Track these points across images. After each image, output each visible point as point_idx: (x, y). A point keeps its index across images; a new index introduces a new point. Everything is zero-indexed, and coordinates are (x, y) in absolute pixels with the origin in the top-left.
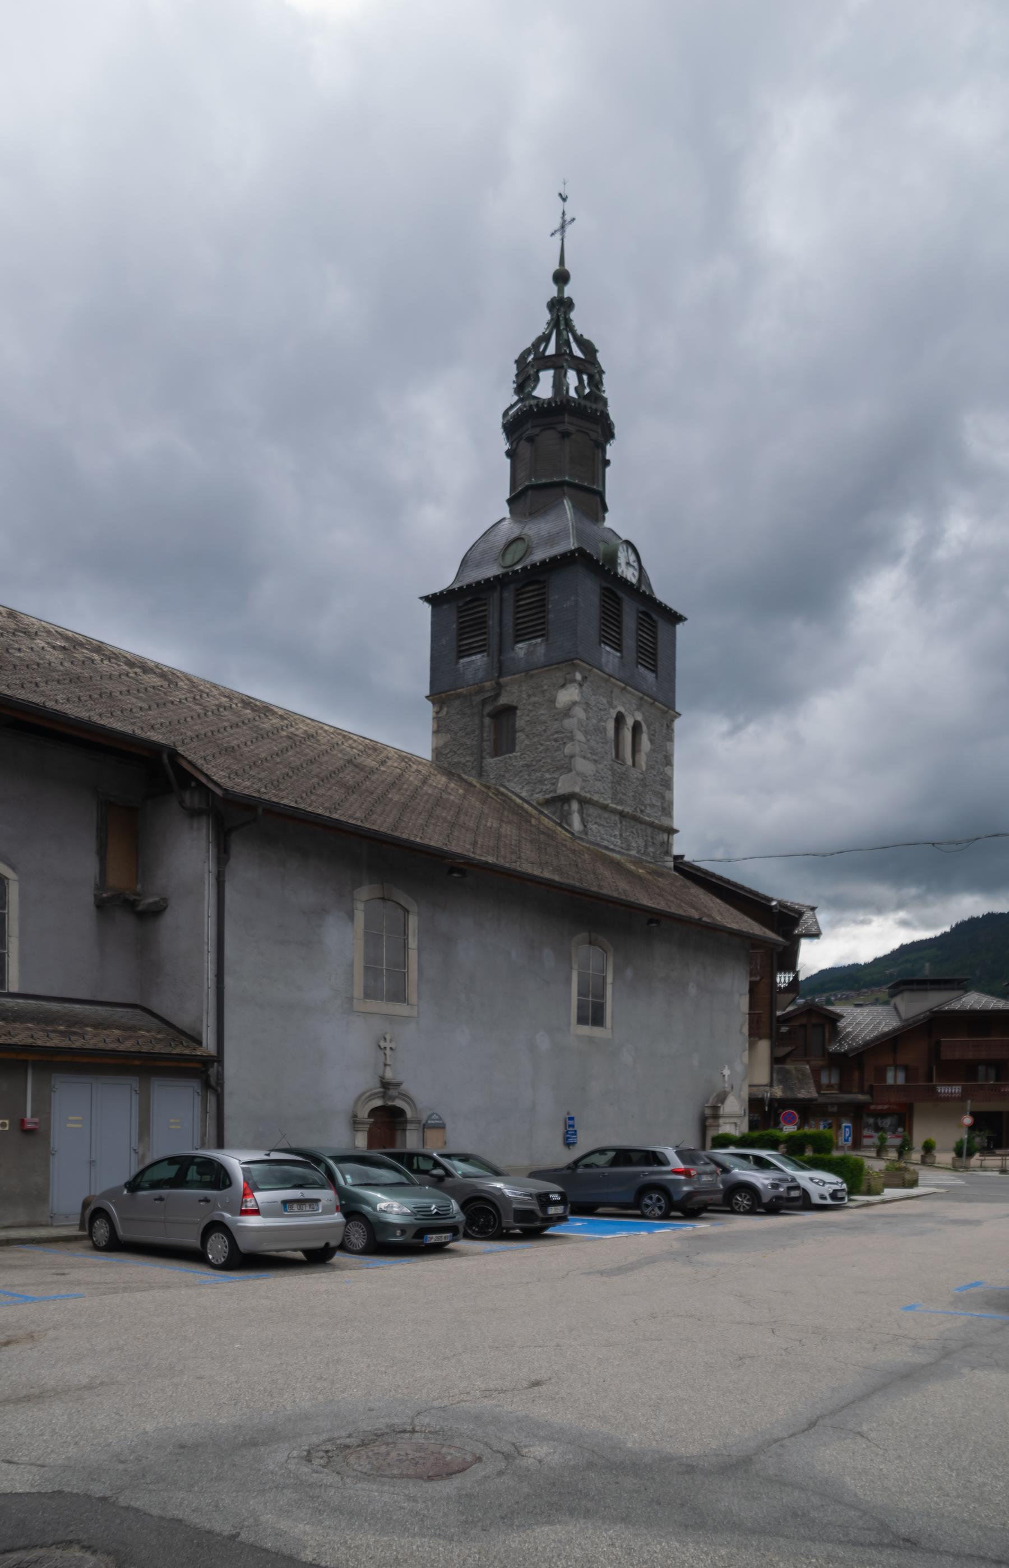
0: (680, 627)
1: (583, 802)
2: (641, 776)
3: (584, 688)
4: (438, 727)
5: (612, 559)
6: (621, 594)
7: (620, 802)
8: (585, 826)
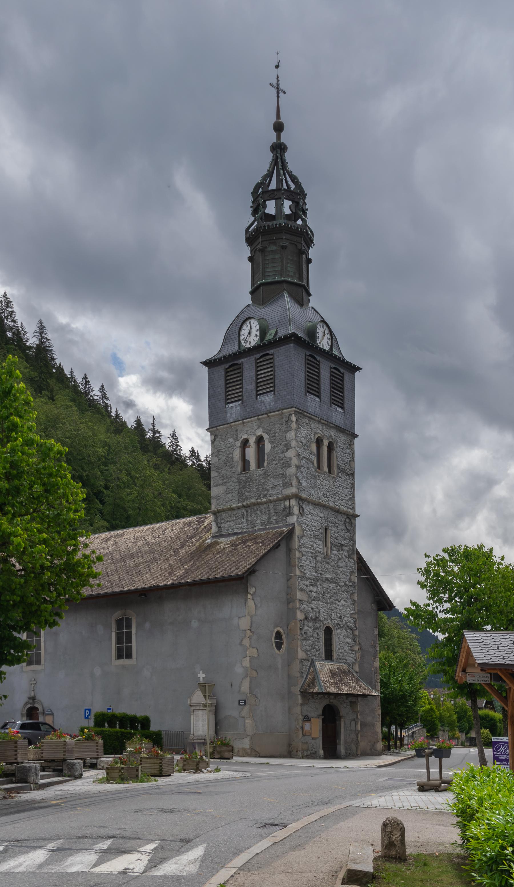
0: (357, 374)
5: (312, 333)
8: (219, 527)
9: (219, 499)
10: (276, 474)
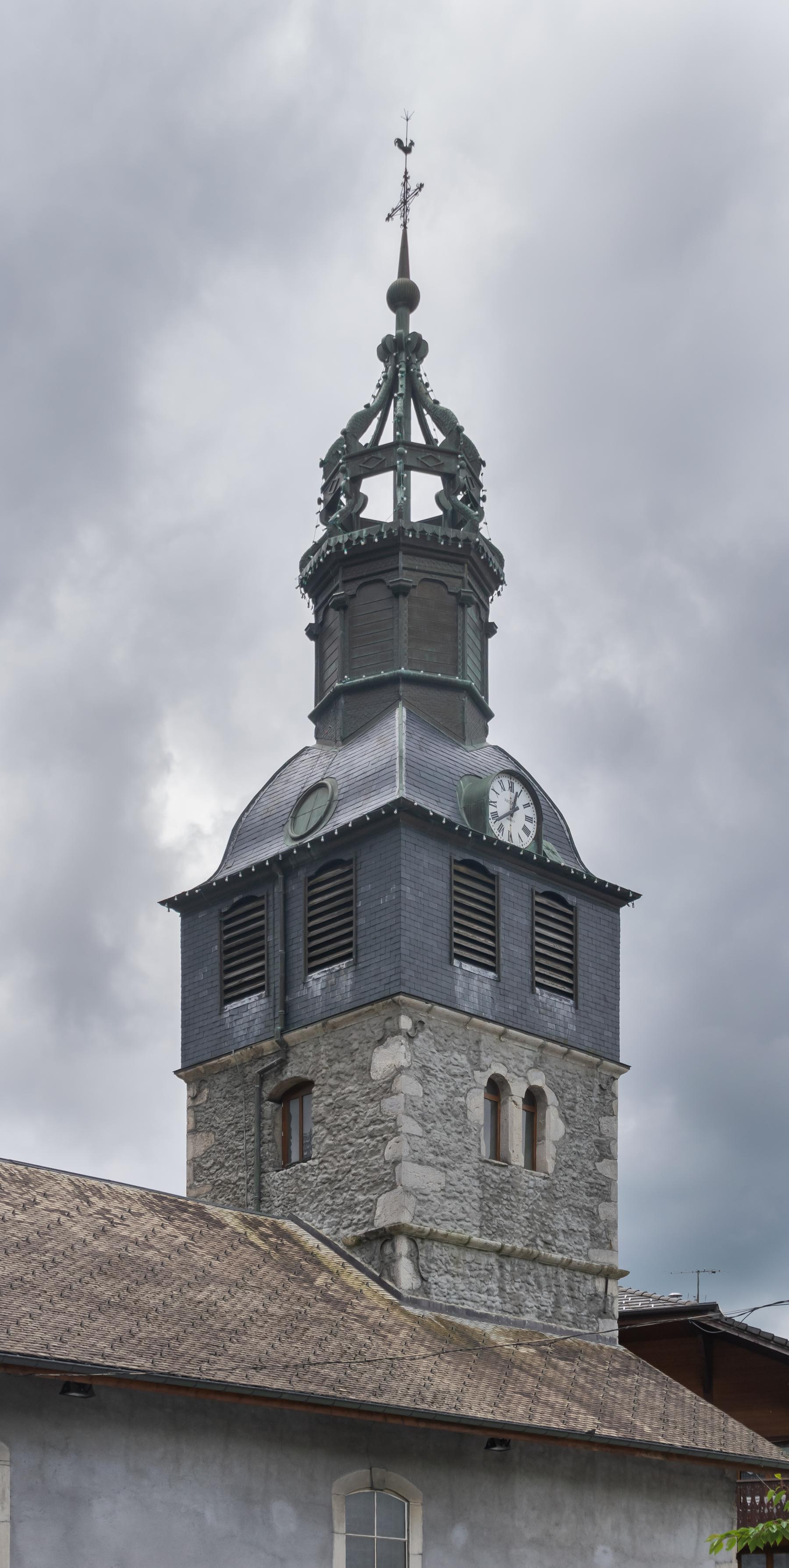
0: (625, 912)
1: (416, 1238)
2: (542, 1183)
3: (417, 1042)
4: (196, 1122)
5: (478, 808)
6: (493, 868)
7: (500, 1232)
8: (423, 1279)
9: (424, 1201)
10: (576, 1203)
